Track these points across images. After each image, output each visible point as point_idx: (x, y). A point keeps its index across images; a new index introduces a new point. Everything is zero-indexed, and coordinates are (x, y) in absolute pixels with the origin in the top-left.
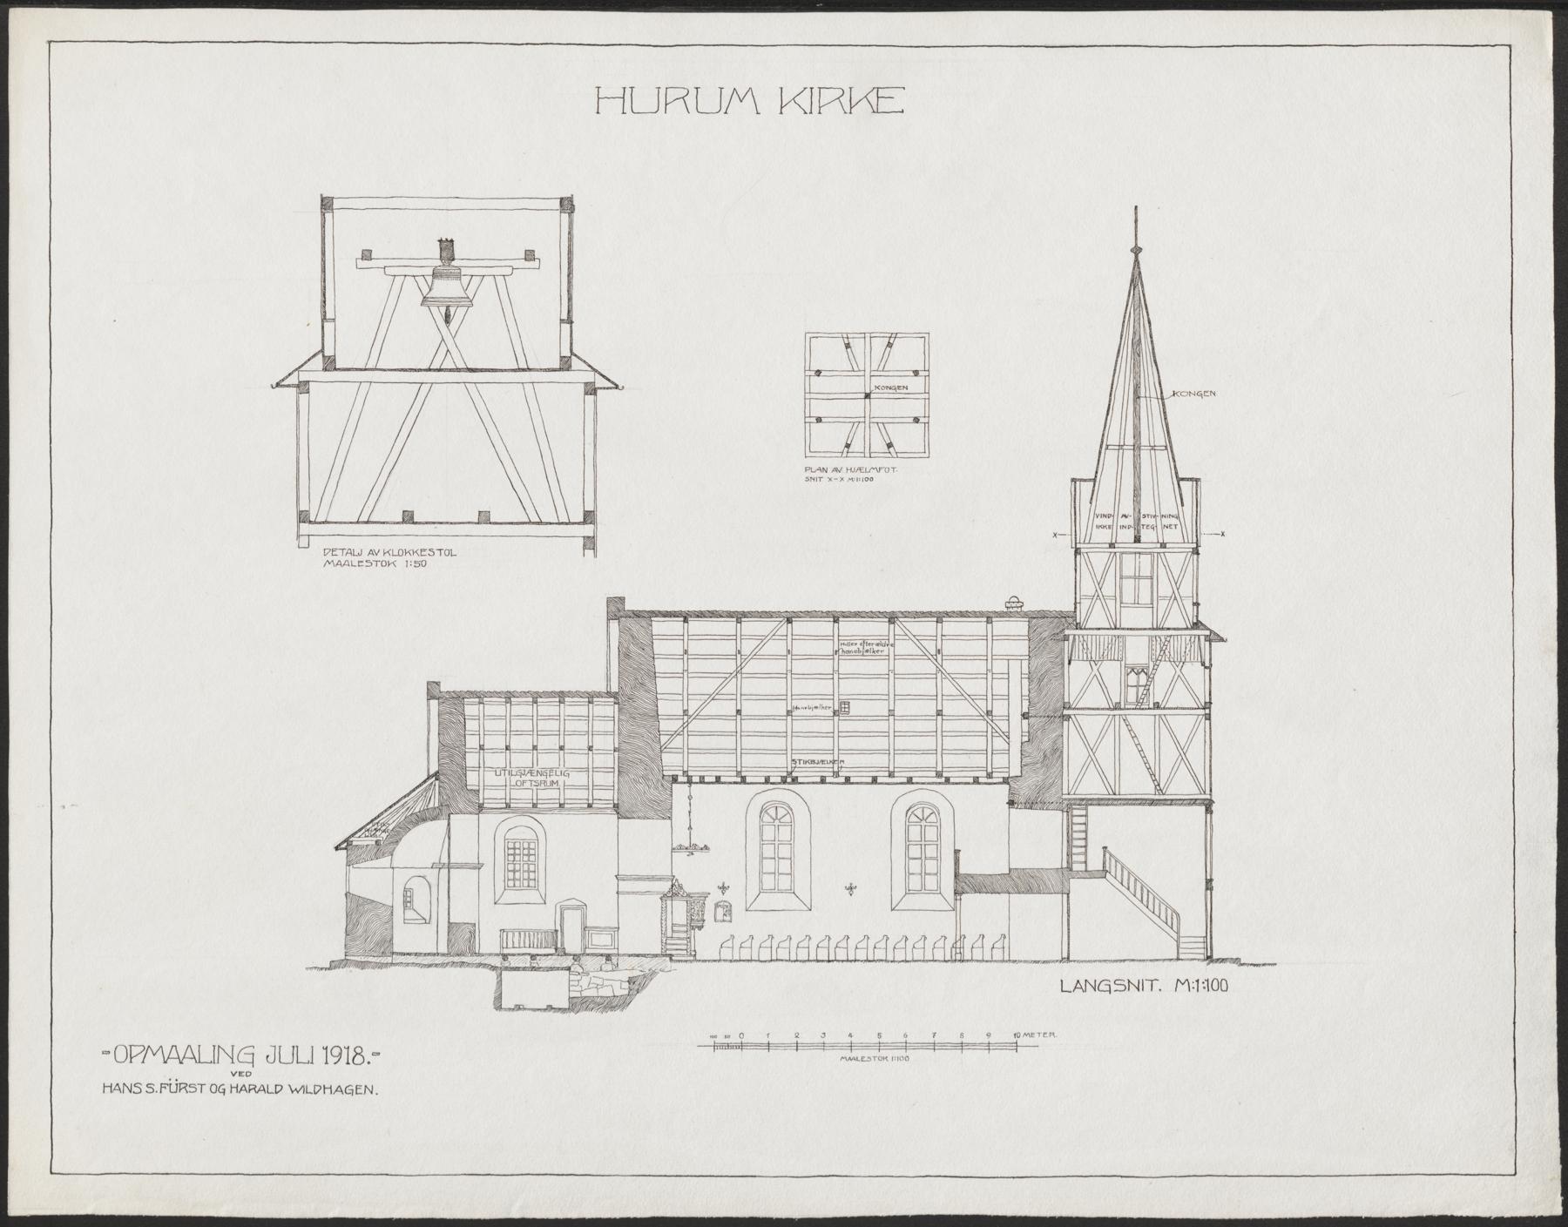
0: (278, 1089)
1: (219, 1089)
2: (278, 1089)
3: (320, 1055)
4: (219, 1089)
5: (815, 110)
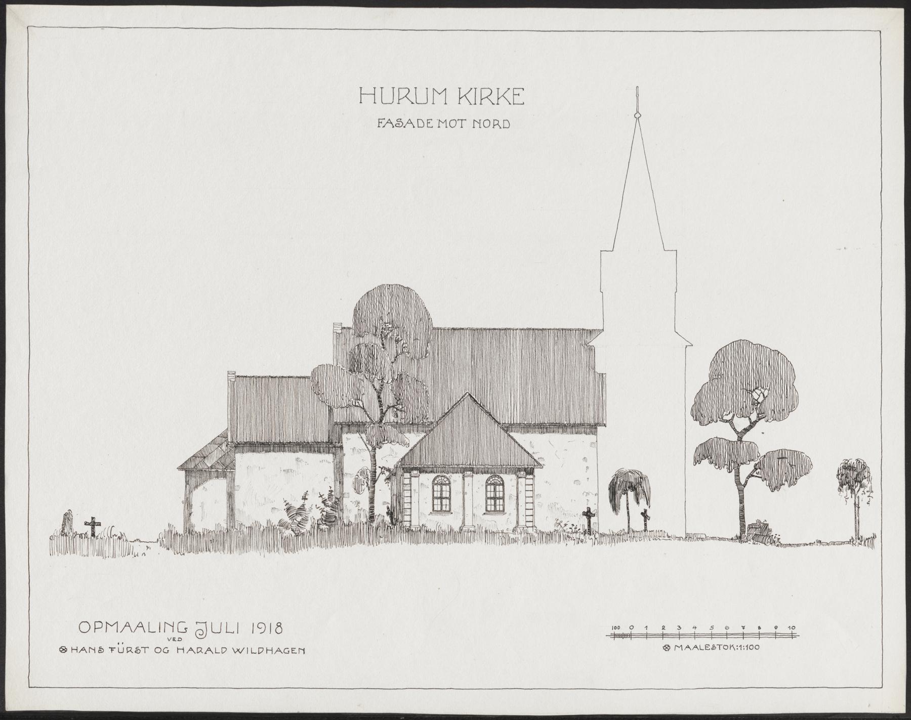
0: (224, 650)
1: (158, 650)
2: (224, 650)
4: (158, 650)
5: (478, 101)
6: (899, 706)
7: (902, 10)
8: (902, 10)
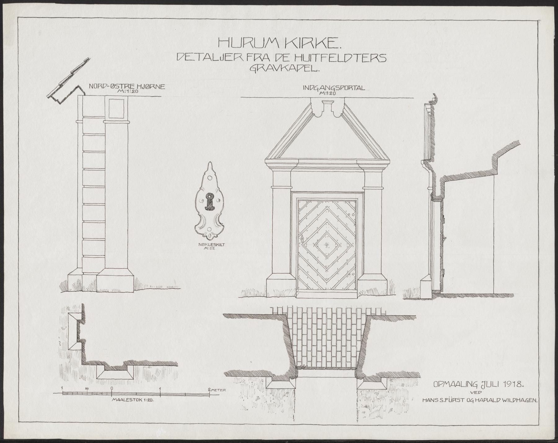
6: (551, 435)
7: (552, 8)
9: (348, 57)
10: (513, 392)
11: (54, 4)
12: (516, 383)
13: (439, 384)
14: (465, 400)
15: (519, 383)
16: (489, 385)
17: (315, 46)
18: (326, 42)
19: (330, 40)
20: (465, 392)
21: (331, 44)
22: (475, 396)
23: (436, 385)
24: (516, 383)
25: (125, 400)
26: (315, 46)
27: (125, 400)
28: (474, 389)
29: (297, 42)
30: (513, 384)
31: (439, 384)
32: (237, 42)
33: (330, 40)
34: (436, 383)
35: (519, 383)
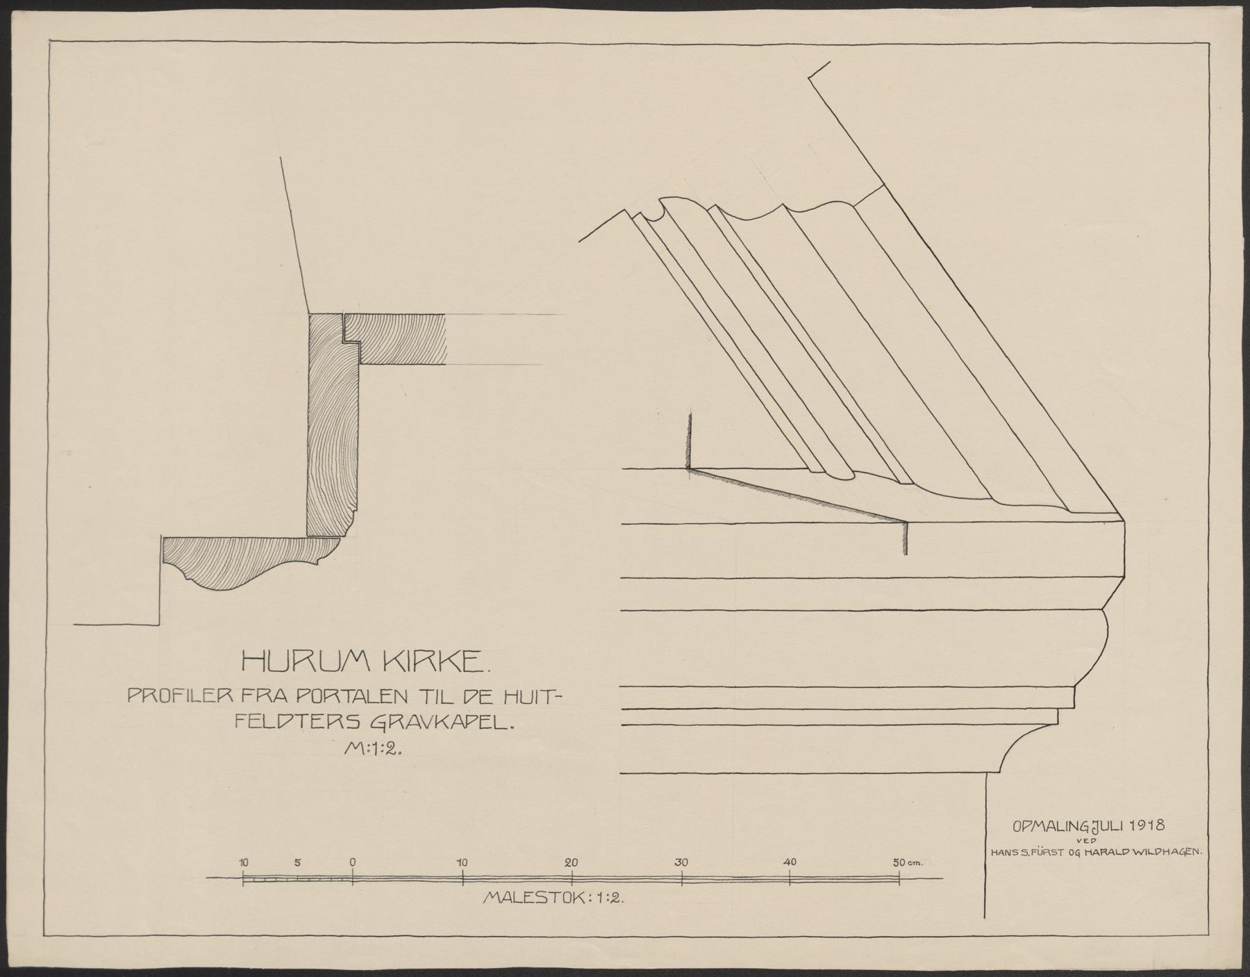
2: (1125, 851)
3: (1127, 826)
6: (1233, 959)
7: (1240, 967)
8: (1240, 967)
9: (470, 719)
10: (1149, 838)
11: (1242, 247)
12: (1155, 824)
13: (1021, 826)
14: (1065, 853)
15: (1160, 822)
16: (1105, 827)
17: (437, 667)
18: (458, 660)
19: (467, 655)
20: (1069, 840)
21: (470, 665)
22: (1083, 847)
23: (1017, 828)
24: (1155, 824)
25: (519, 897)
26: (437, 667)
27: (519, 897)
28: (1083, 835)
29: (403, 659)
30: (1148, 826)
31: (1021, 826)
32: (278, 661)
33: (467, 655)
34: (1017, 825)
35: (1160, 822)
